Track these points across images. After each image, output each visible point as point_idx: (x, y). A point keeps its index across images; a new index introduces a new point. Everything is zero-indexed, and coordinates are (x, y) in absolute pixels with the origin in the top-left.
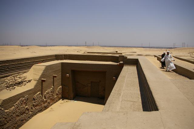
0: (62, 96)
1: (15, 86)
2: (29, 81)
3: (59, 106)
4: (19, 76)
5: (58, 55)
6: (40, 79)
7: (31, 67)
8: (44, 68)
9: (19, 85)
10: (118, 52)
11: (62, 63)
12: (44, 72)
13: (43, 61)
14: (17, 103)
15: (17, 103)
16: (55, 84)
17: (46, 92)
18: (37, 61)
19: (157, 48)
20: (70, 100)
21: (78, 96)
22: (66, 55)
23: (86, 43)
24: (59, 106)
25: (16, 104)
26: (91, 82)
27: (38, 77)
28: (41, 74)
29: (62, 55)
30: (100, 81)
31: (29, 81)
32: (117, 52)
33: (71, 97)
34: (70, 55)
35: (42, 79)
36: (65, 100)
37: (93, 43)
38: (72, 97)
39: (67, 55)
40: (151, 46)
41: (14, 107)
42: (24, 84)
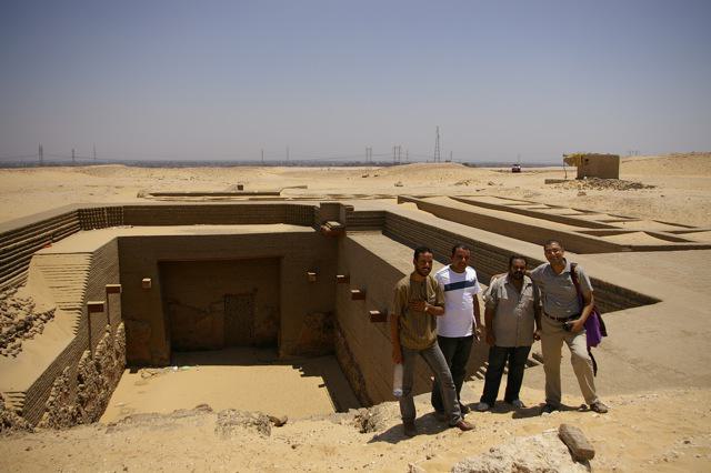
0: (127, 360)
1: (18, 341)
2: (50, 315)
3: (140, 393)
4: (9, 301)
5: (89, 210)
6: (84, 303)
7: (26, 262)
8: (84, 261)
9: (26, 334)
10: (246, 189)
11: (121, 241)
12: (90, 277)
13: (54, 235)
14: (51, 399)
15: (51, 399)
16: (111, 318)
17: (99, 347)
18: (39, 239)
19: (313, 166)
20: (162, 366)
21: (185, 350)
22: (117, 208)
23: (41, 150)
24: (140, 393)
25: (52, 404)
26: (226, 296)
27: (76, 298)
28: (82, 286)
29: (99, 211)
30: (256, 290)
31: (50, 315)
32: (241, 187)
33: (162, 359)
34: (132, 207)
35: (89, 303)
36: (146, 372)
37: (73, 151)
38: (166, 356)
39: (120, 208)
40: (292, 158)
41: (46, 414)
42: (38, 329)
